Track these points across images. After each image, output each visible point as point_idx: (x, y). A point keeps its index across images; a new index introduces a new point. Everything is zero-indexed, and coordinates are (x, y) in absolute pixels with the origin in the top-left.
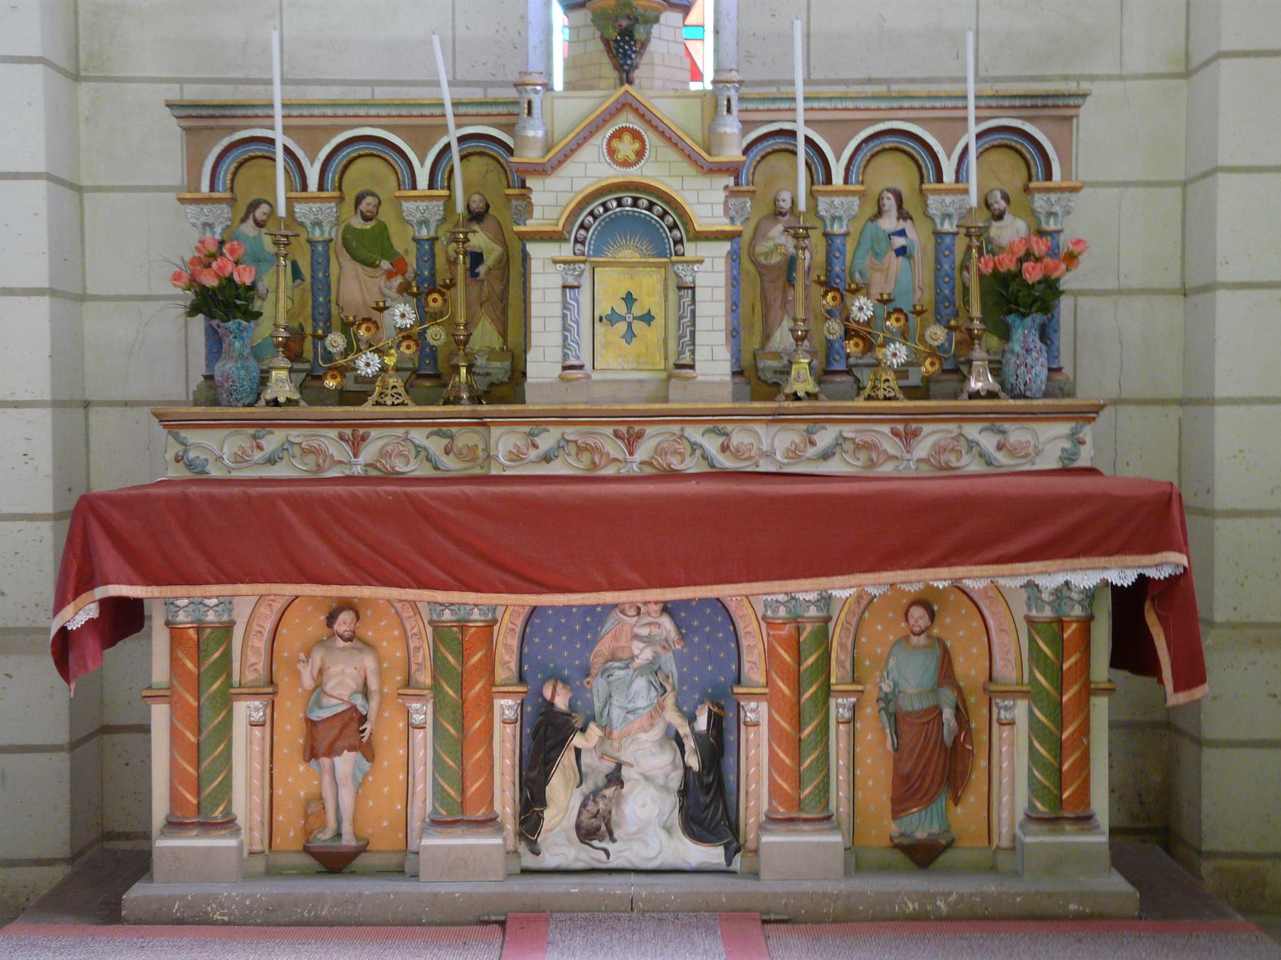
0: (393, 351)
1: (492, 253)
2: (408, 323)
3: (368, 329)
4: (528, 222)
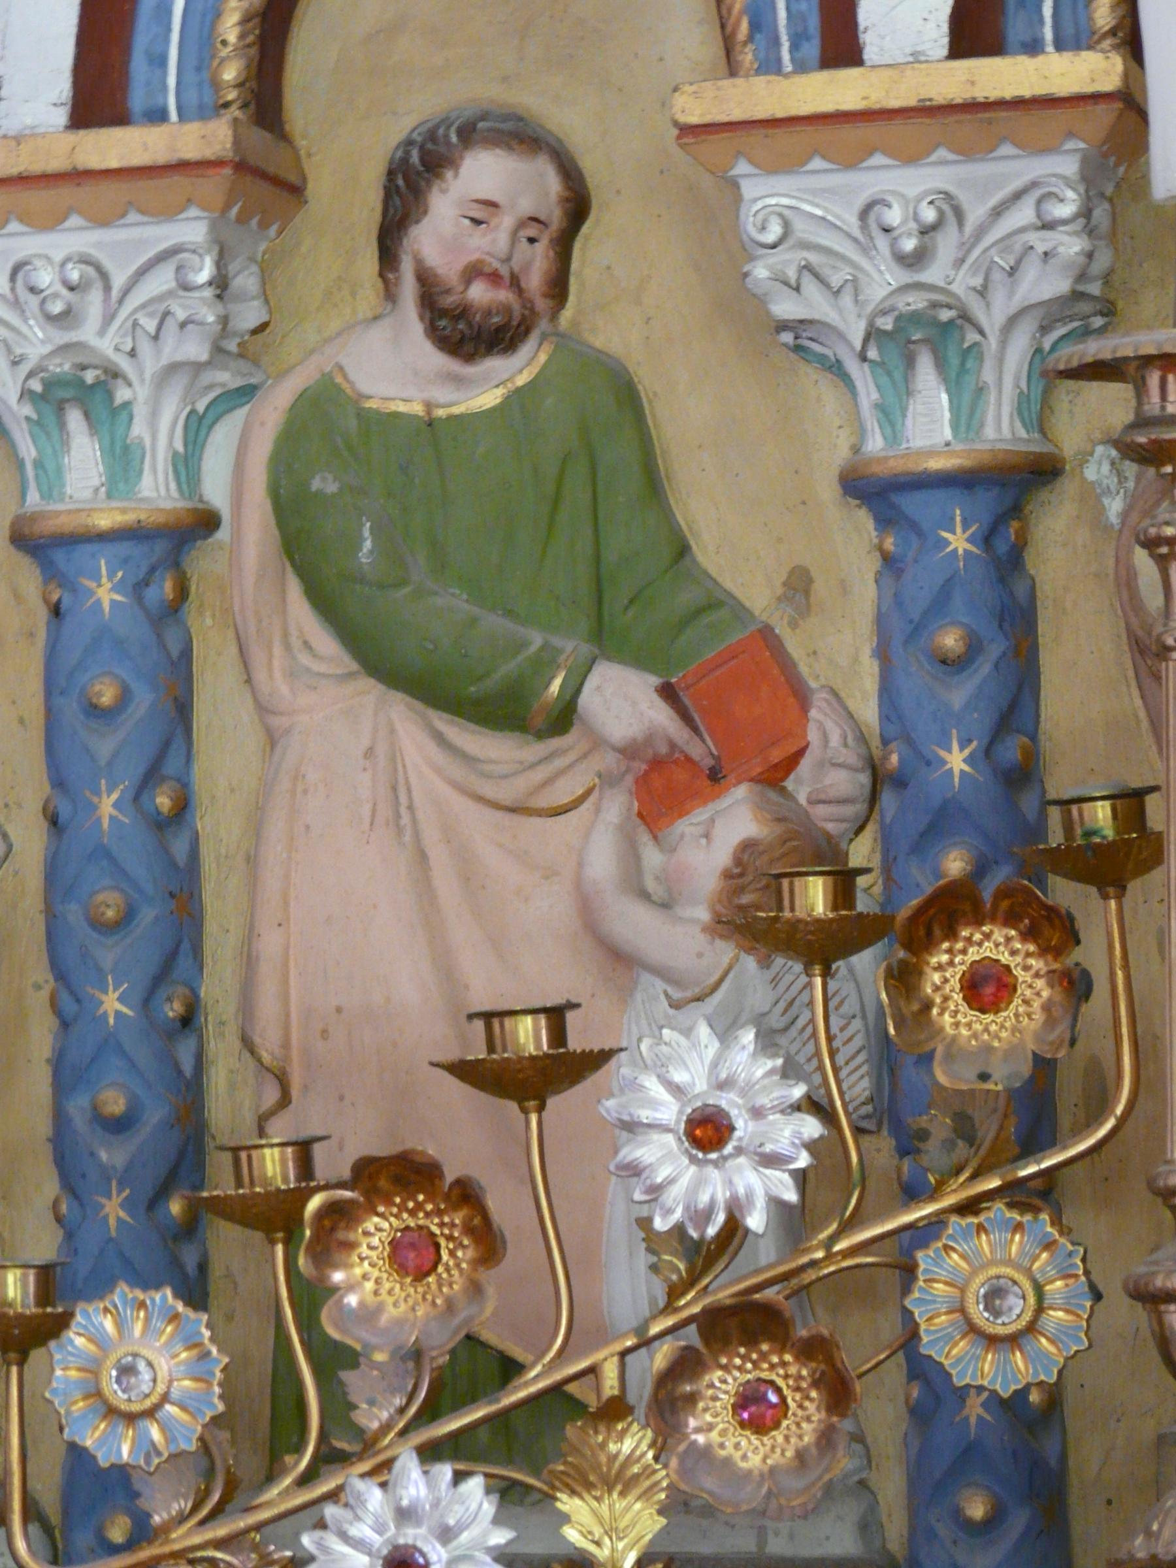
0: (631, 1443)
2: (753, 1186)
3: (413, 1258)
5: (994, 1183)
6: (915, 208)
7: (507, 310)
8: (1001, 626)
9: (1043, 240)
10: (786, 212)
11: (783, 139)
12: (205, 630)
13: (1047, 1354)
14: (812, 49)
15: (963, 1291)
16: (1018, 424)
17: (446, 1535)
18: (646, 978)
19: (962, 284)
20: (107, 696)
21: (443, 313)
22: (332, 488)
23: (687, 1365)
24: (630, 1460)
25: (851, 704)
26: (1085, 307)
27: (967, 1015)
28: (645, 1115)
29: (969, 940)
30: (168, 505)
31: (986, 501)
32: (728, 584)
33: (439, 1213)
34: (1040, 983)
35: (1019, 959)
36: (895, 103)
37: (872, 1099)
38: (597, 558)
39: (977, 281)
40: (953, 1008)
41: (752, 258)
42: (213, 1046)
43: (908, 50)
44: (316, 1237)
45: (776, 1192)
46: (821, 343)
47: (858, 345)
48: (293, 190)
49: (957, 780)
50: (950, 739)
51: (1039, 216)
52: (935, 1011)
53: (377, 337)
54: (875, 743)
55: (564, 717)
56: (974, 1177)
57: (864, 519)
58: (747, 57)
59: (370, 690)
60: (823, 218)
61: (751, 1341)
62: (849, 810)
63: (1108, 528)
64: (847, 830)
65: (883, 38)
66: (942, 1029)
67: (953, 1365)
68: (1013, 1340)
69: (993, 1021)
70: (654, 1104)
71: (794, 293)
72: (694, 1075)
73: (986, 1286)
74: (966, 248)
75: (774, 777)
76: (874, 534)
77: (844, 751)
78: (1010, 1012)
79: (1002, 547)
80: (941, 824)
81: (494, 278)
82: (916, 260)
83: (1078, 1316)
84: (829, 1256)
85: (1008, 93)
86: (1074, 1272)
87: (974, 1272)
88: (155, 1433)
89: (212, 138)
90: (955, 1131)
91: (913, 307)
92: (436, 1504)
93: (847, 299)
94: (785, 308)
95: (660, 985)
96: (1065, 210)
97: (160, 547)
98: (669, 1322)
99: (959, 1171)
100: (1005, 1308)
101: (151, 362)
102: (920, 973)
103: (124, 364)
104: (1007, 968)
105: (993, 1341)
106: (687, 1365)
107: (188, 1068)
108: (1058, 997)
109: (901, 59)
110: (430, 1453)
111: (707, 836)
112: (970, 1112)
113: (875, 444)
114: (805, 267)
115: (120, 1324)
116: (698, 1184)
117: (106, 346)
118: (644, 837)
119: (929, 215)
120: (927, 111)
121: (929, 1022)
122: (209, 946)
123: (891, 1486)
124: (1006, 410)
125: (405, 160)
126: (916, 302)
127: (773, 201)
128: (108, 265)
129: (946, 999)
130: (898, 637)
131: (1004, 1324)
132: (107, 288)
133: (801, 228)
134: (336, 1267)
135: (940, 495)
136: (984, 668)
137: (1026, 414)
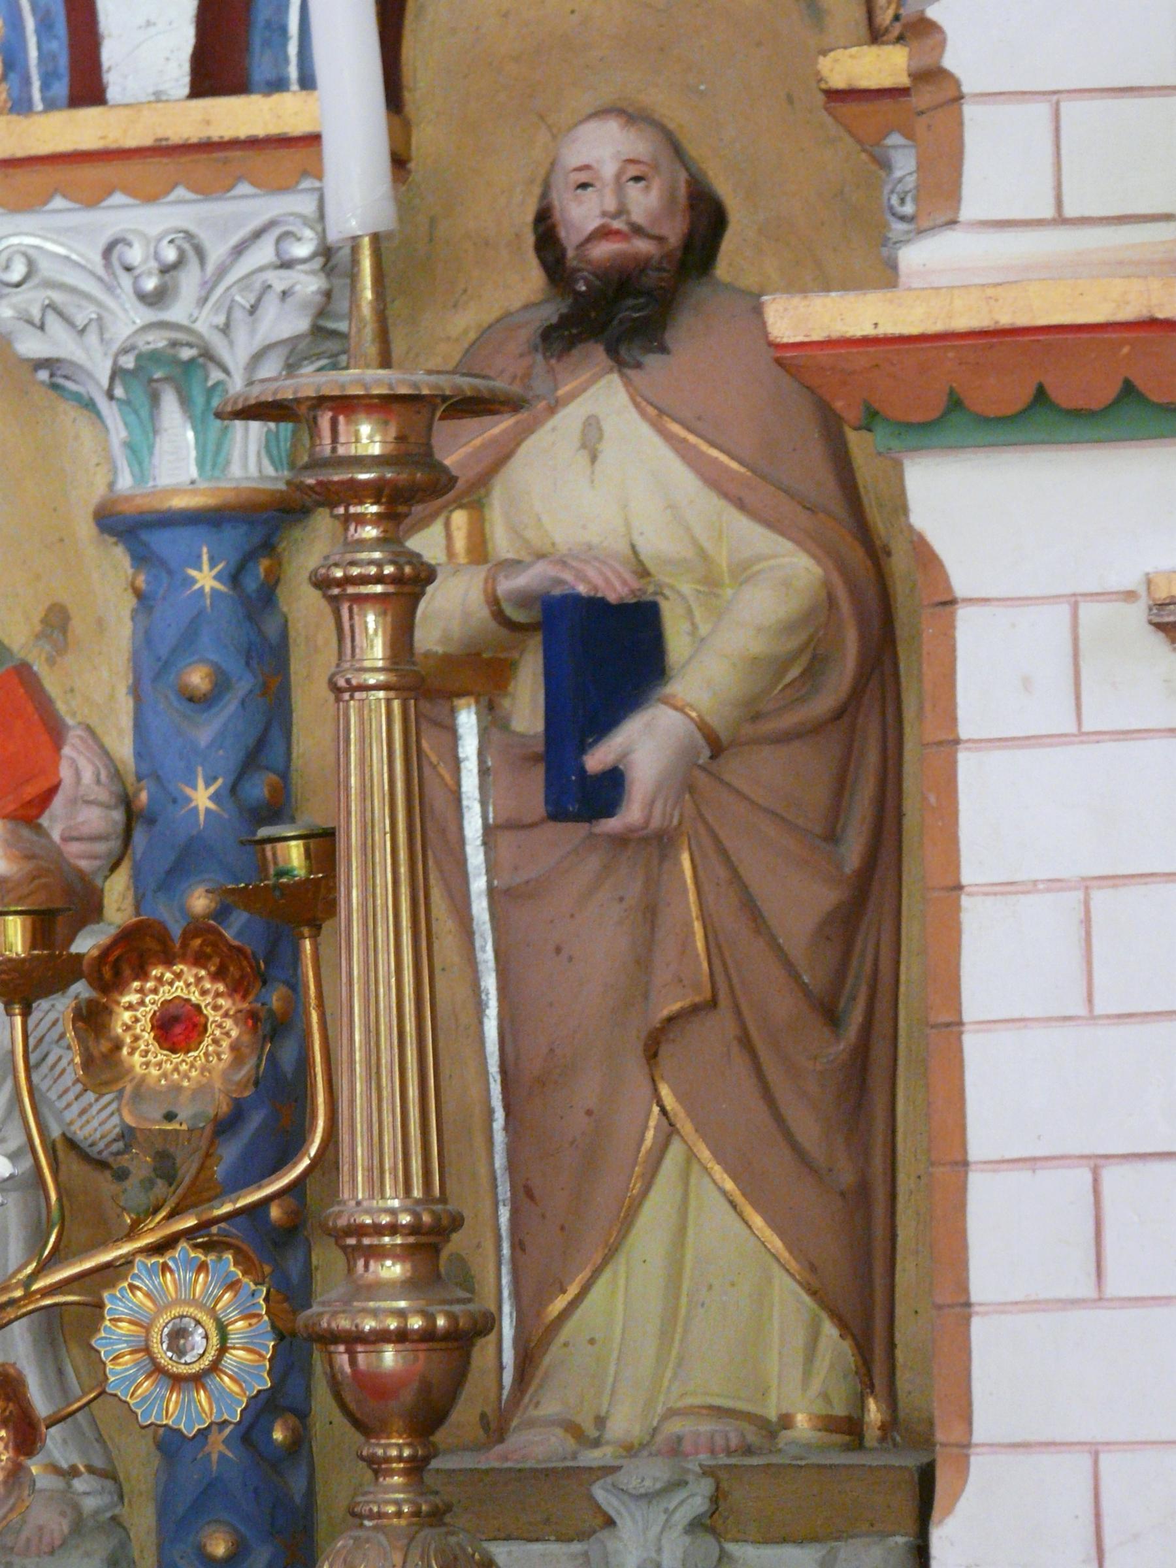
1: (739, 611)
4: (919, 257)
5: (191, 1222)
6: (156, 247)
8: (248, 664)
9: (281, 279)
10: (31, 252)
13: (231, 1394)
14: (61, 89)
15: (148, 1329)
16: (266, 462)
19: (206, 323)
25: (108, 741)
29: (159, 980)
31: (235, 538)
34: (228, 1023)
35: (209, 999)
36: (131, 143)
37: (123, 1136)
39: (221, 320)
40: (143, 1047)
43: (151, 90)
46: (74, 381)
47: (105, 382)
49: (202, 818)
50: (196, 778)
51: (278, 254)
52: (125, 1051)
54: (130, 779)
56: (171, 1216)
57: (120, 555)
60: (67, 258)
62: (101, 848)
64: (99, 868)
65: (125, 77)
66: (132, 1068)
67: (138, 1405)
68: (198, 1379)
69: (183, 1061)
71: (39, 332)
73: (170, 1325)
74: (208, 288)
76: (130, 571)
77: (96, 788)
78: (199, 1053)
79: (251, 585)
80: (185, 862)
82: (156, 299)
83: (261, 1355)
84: (28, 1295)
85: (243, 133)
86: (258, 1312)
87: (160, 1310)
90: (155, 1170)
91: (152, 346)
93: (92, 337)
94: (30, 346)
96: (302, 250)
99: (156, 1211)
100: (189, 1347)
102: (110, 1013)
104: (198, 1008)
105: (177, 1381)
108: (246, 1038)
109: (143, 98)
112: (172, 1150)
113: (125, 482)
114: (48, 306)
119: (171, 255)
120: (162, 150)
121: (119, 1063)
123: (142, 1521)
124: (253, 448)
126: (157, 341)
127: (15, 240)
129: (136, 1038)
130: (152, 671)
131: (186, 1364)
133: (46, 269)
136: (230, 706)
137: (275, 452)
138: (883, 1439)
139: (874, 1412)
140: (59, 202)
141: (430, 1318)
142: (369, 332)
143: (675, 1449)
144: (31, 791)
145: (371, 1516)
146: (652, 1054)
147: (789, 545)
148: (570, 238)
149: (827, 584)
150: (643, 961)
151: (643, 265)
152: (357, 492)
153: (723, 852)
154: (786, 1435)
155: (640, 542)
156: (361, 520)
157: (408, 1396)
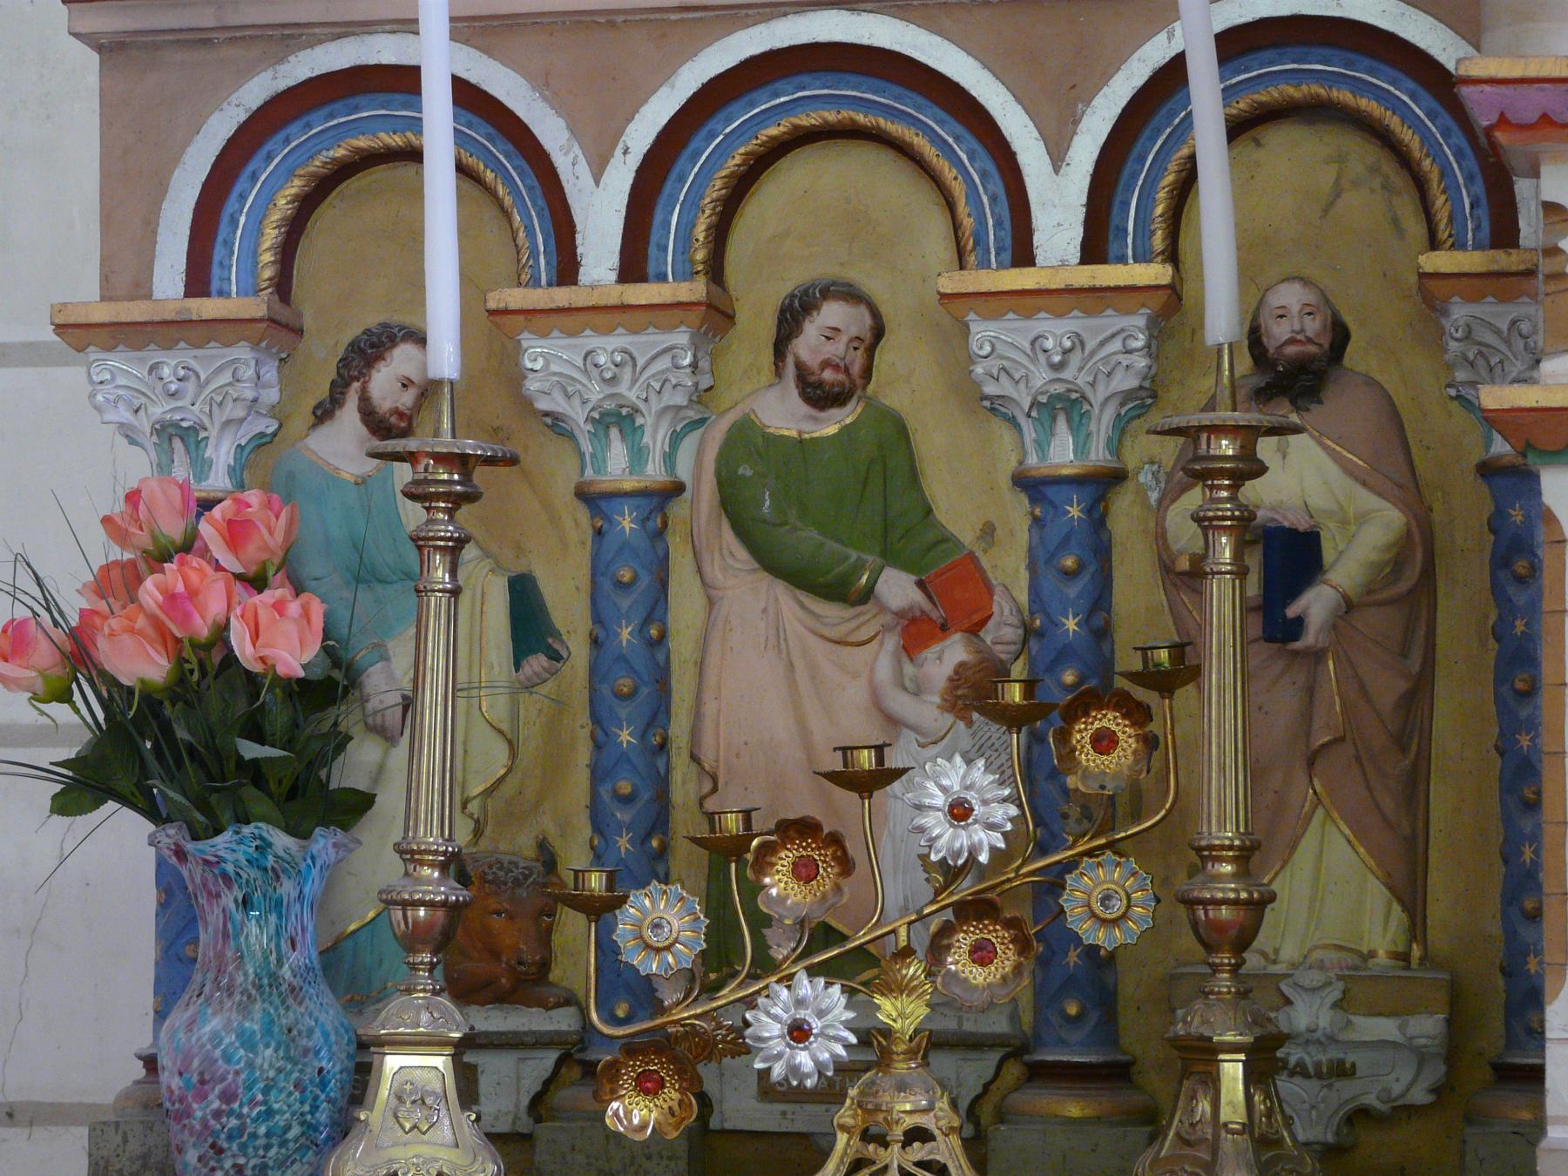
0: (914, 969)
2: (983, 840)
3: (804, 872)
5: (1103, 841)
7: (842, 384)
11: (993, 303)
12: (678, 547)
14: (1007, 256)
17: (821, 1014)
18: (905, 731)
19: (1083, 380)
20: (626, 576)
21: (810, 385)
22: (749, 473)
23: (947, 930)
24: (913, 978)
26: (1144, 394)
27: (1092, 754)
28: (927, 801)
30: (661, 479)
32: (950, 527)
33: (819, 849)
38: (886, 513)
39: (1090, 379)
41: (974, 363)
42: (675, 760)
44: (756, 859)
45: (994, 842)
48: (729, 317)
53: (772, 396)
54: (1026, 613)
55: (867, 595)
58: (972, 259)
59: (765, 579)
61: (979, 919)
62: (1013, 648)
63: (1149, 507)
68: (1114, 922)
70: (932, 796)
72: (953, 781)
74: (1085, 361)
75: (974, 630)
79: (1096, 515)
80: (1064, 655)
81: (836, 367)
84: (1017, 877)
87: (1096, 886)
88: (670, 959)
89: (696, 290)
92: (816, 998)
93: (1022, 386)
94: (990, 389)
95: (913, 735)
96: (1139, 344)
97: (655, 501)
98: (934, 907)
101: (655, 405)
102: (1070, 734)
103: (642, 406)
105: (1104, 922)
106: (947, 930)
107: (662, 771)
110: (812, 972)
111: (939, 658)
113: (1032, 460)
115: (652, 903)
116: (954, 838)
117: (632, 395)
118: (905, 659)
119: (1068, 344)
122: (674, 708)
125: (791, 304)
126: (1059, 388)
128: (636, 354)
132: (635, 365)
133: (999, 346)
134: (765, 875)
135: (1065, 487)
136: (1086, 577)
138: (1420, 964)
139: (1416, 951)
140: (1011, 316)
141: (1251, 894)
142: (1227, 392)
143: (1321, 966)
144: (976, 618)
145: (1212, 992)
146: (1311, 763)
147: (1388, 505)
148: (1271, 345)
149: (1407, 524)
150: (1307, 716)
151: (1312, 358)
152: (1222, 473)
153: (1351, 663)
154: (1371, 962)
155: (1309, 501)
156: (1220, 488)
157: (1233, 933)
